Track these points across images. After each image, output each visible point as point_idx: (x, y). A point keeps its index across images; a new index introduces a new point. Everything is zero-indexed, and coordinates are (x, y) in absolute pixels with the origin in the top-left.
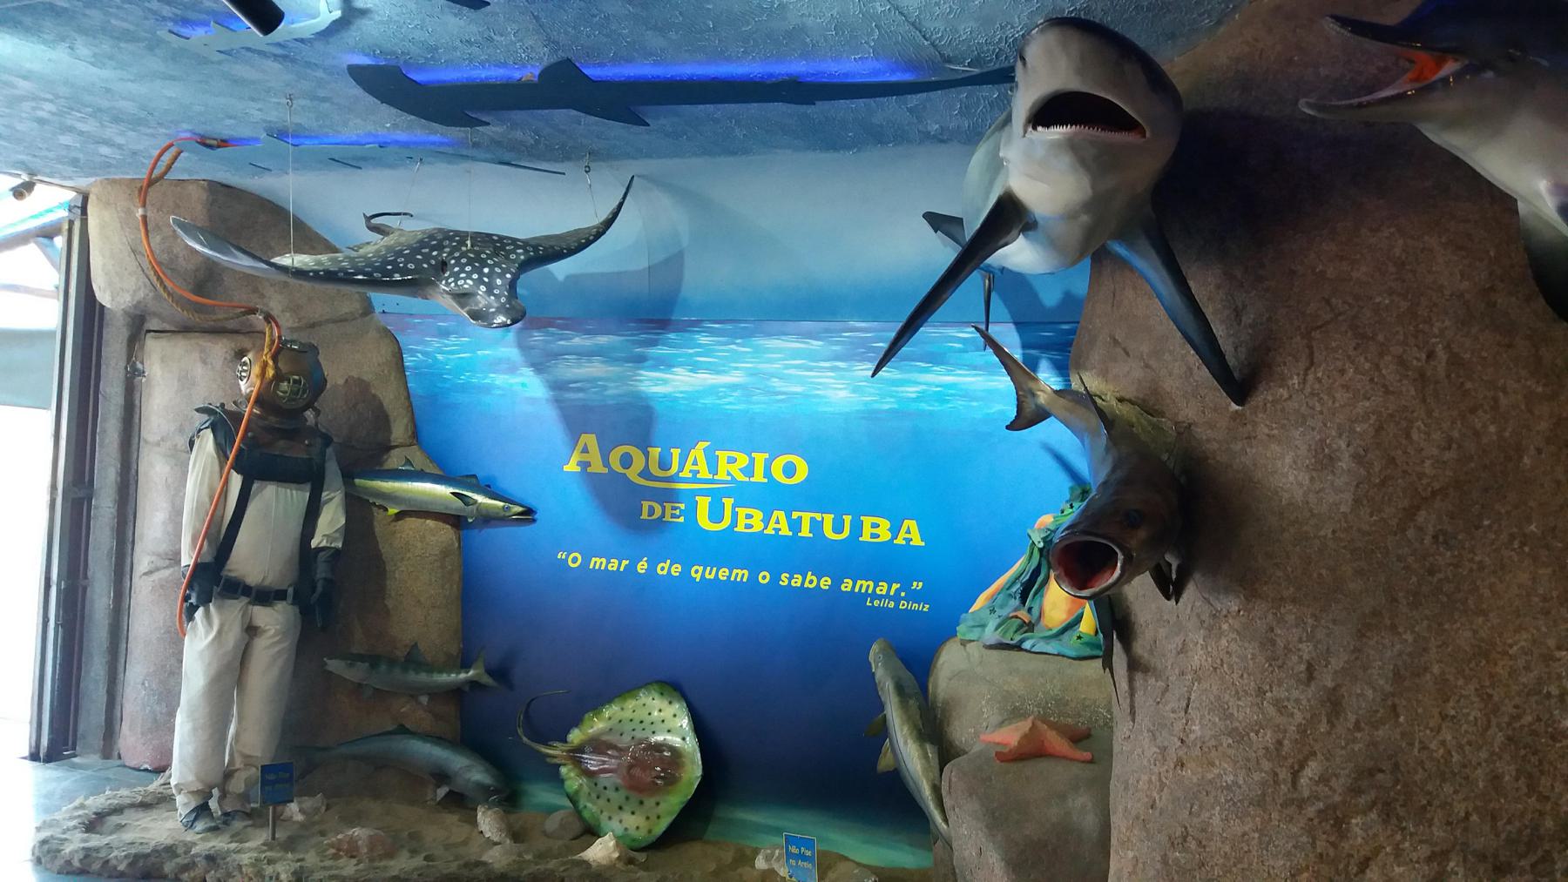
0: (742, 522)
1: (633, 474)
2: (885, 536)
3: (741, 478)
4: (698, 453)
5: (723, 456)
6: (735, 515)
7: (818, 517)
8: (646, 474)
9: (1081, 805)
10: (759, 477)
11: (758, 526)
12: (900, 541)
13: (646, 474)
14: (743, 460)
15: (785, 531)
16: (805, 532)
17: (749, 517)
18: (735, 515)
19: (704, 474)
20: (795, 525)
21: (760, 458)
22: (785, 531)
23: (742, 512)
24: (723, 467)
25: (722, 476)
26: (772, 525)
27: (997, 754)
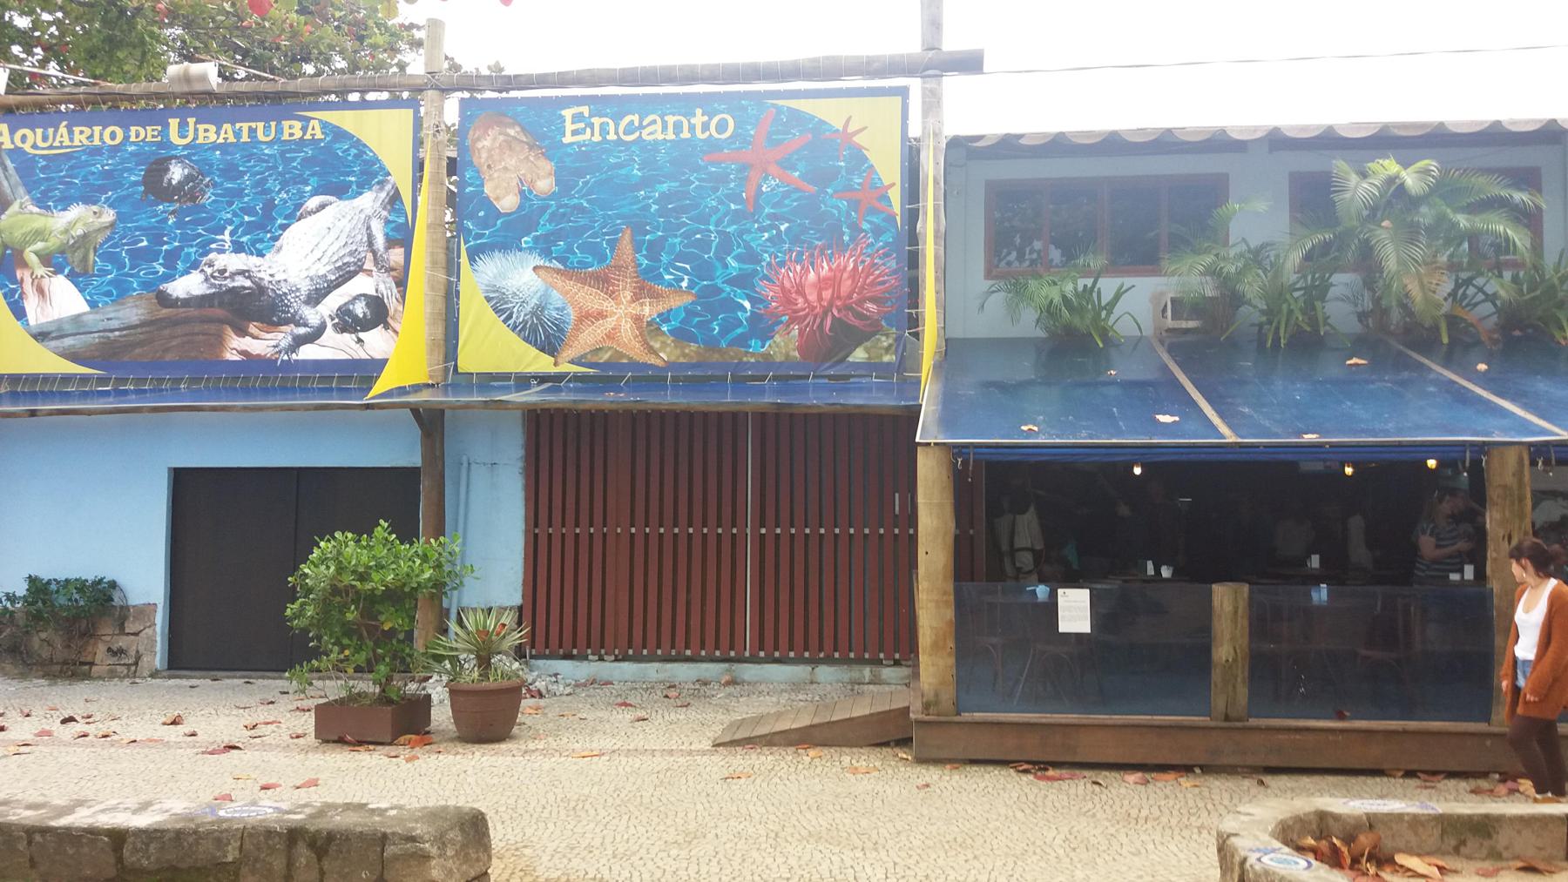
0: (201, 134)
1: (27, 147)
2: (298, 134)
3: (86, 142)
4: (63, 130)
5: (77, 130)
6: (196, 130)
7: (253, 125)
8: (35, 146)
9: (1511, 457)
10: (97, 142)
11: (212, 137)
12: (308, 137)
13: (35, 146)
14: (87, 131)
15: (232, 139)
16: (245, 138)
17: (206, 131)
18: (196, 130)
19: (67, 143)
20: (237, 134)
21: (97, 129)
22: (232, 139)
23: (201, 127)
24: (77, 136)
25: (77, 143)
26: (222, 135)
27: (1367, 241)
